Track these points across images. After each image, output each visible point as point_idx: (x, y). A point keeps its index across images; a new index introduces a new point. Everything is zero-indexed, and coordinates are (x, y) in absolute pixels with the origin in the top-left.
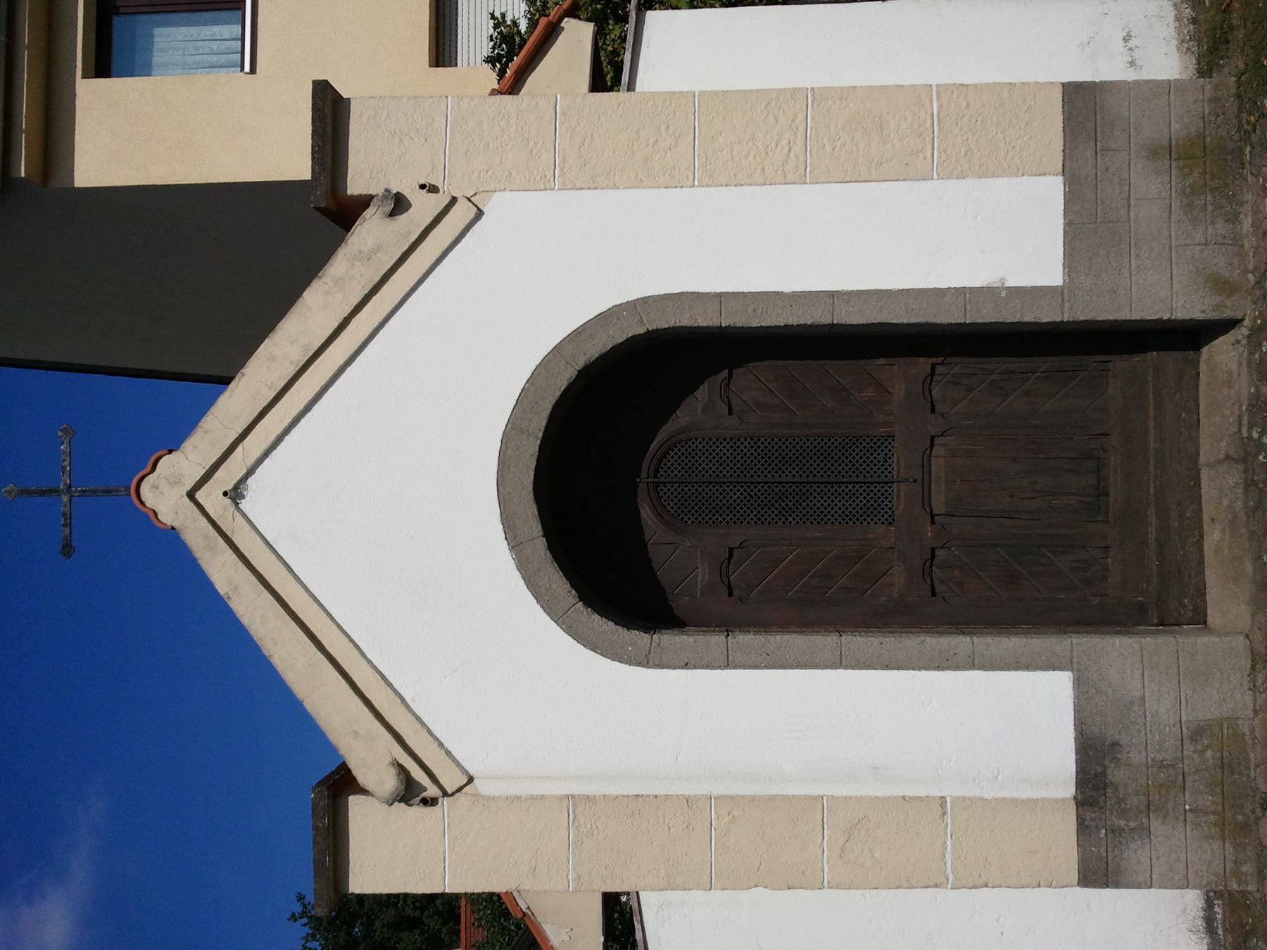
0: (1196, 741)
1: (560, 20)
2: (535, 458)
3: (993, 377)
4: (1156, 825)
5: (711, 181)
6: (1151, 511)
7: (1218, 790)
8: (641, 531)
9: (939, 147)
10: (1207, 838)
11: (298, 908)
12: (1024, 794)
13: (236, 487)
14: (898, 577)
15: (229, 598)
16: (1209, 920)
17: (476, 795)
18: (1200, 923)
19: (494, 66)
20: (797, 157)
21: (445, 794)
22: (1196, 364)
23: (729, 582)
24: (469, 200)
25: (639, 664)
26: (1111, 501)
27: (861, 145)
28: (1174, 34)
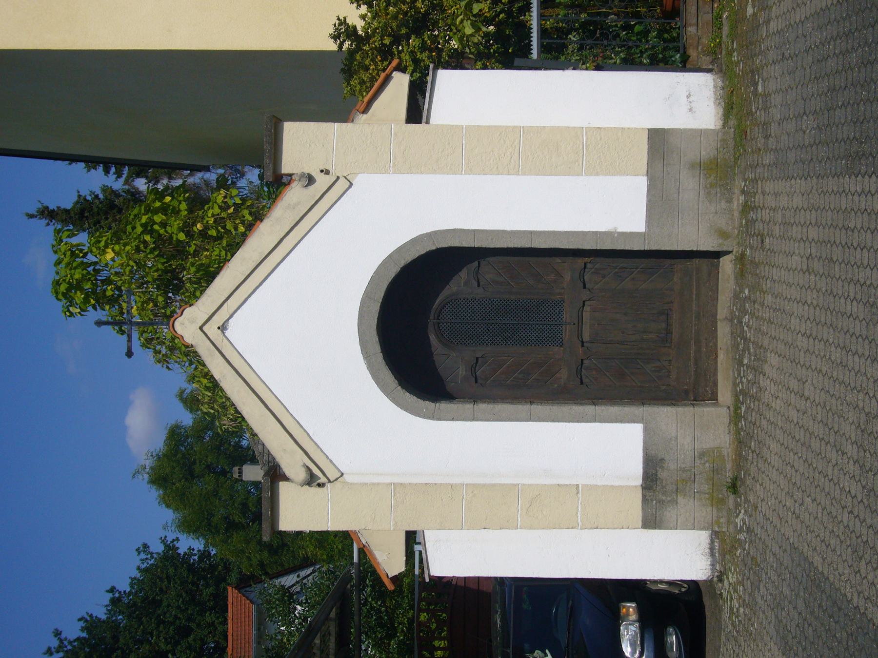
0: (701, 458)
1: (391, 73)
2: (378, 313)
3: (616, 270)
4: (680, 499)
5: (470, 171)
6: (692, 342)
7: (711, 483)
8: (431, 354)
9: (586, 159)
10: (704, 505)
11: (55, 643)
12: (617, 483)
13: (224, 324)
14: (563, 374)
15: (220, 381)
16: (712, 549)
17: (345, 482)
18: (707, 551)
19: (336, 41)
20: (515, 162)
21: (330, 481)
22: (717, 267)
23: (476, 375)
24: (345, 177)
25: (429, 418)
26: (673, 336)
27: (547, 157)
28: (713, 95)
